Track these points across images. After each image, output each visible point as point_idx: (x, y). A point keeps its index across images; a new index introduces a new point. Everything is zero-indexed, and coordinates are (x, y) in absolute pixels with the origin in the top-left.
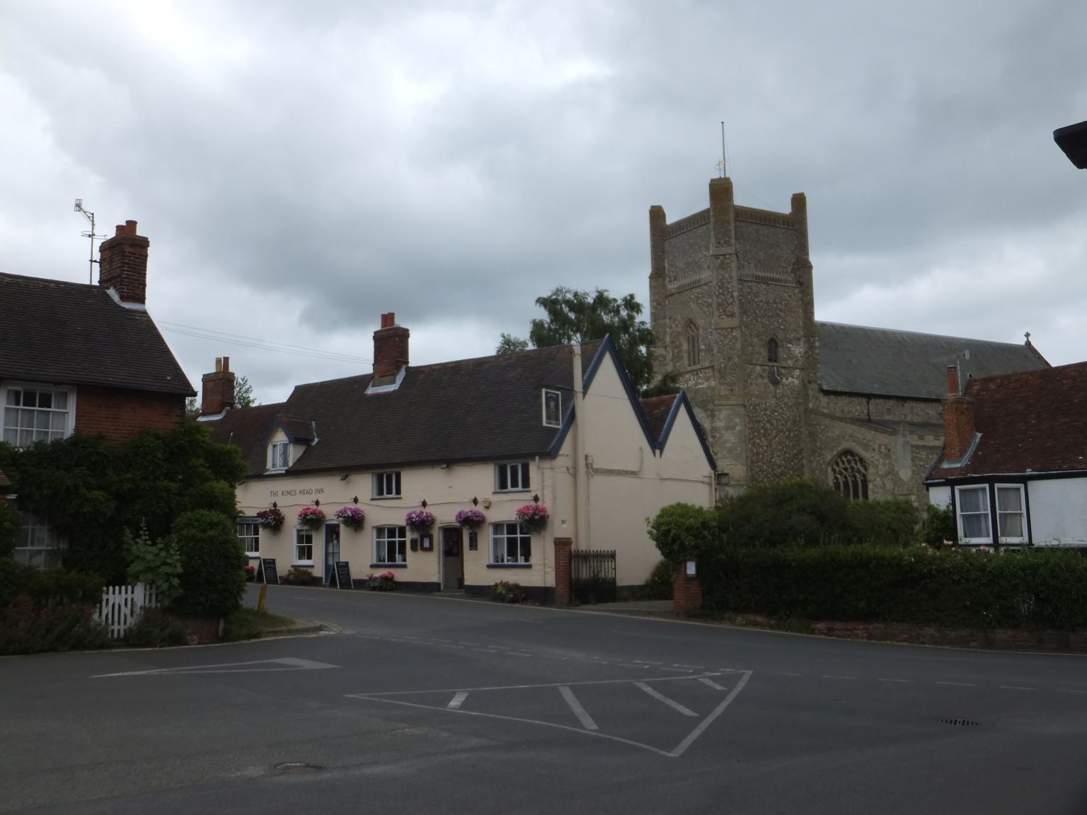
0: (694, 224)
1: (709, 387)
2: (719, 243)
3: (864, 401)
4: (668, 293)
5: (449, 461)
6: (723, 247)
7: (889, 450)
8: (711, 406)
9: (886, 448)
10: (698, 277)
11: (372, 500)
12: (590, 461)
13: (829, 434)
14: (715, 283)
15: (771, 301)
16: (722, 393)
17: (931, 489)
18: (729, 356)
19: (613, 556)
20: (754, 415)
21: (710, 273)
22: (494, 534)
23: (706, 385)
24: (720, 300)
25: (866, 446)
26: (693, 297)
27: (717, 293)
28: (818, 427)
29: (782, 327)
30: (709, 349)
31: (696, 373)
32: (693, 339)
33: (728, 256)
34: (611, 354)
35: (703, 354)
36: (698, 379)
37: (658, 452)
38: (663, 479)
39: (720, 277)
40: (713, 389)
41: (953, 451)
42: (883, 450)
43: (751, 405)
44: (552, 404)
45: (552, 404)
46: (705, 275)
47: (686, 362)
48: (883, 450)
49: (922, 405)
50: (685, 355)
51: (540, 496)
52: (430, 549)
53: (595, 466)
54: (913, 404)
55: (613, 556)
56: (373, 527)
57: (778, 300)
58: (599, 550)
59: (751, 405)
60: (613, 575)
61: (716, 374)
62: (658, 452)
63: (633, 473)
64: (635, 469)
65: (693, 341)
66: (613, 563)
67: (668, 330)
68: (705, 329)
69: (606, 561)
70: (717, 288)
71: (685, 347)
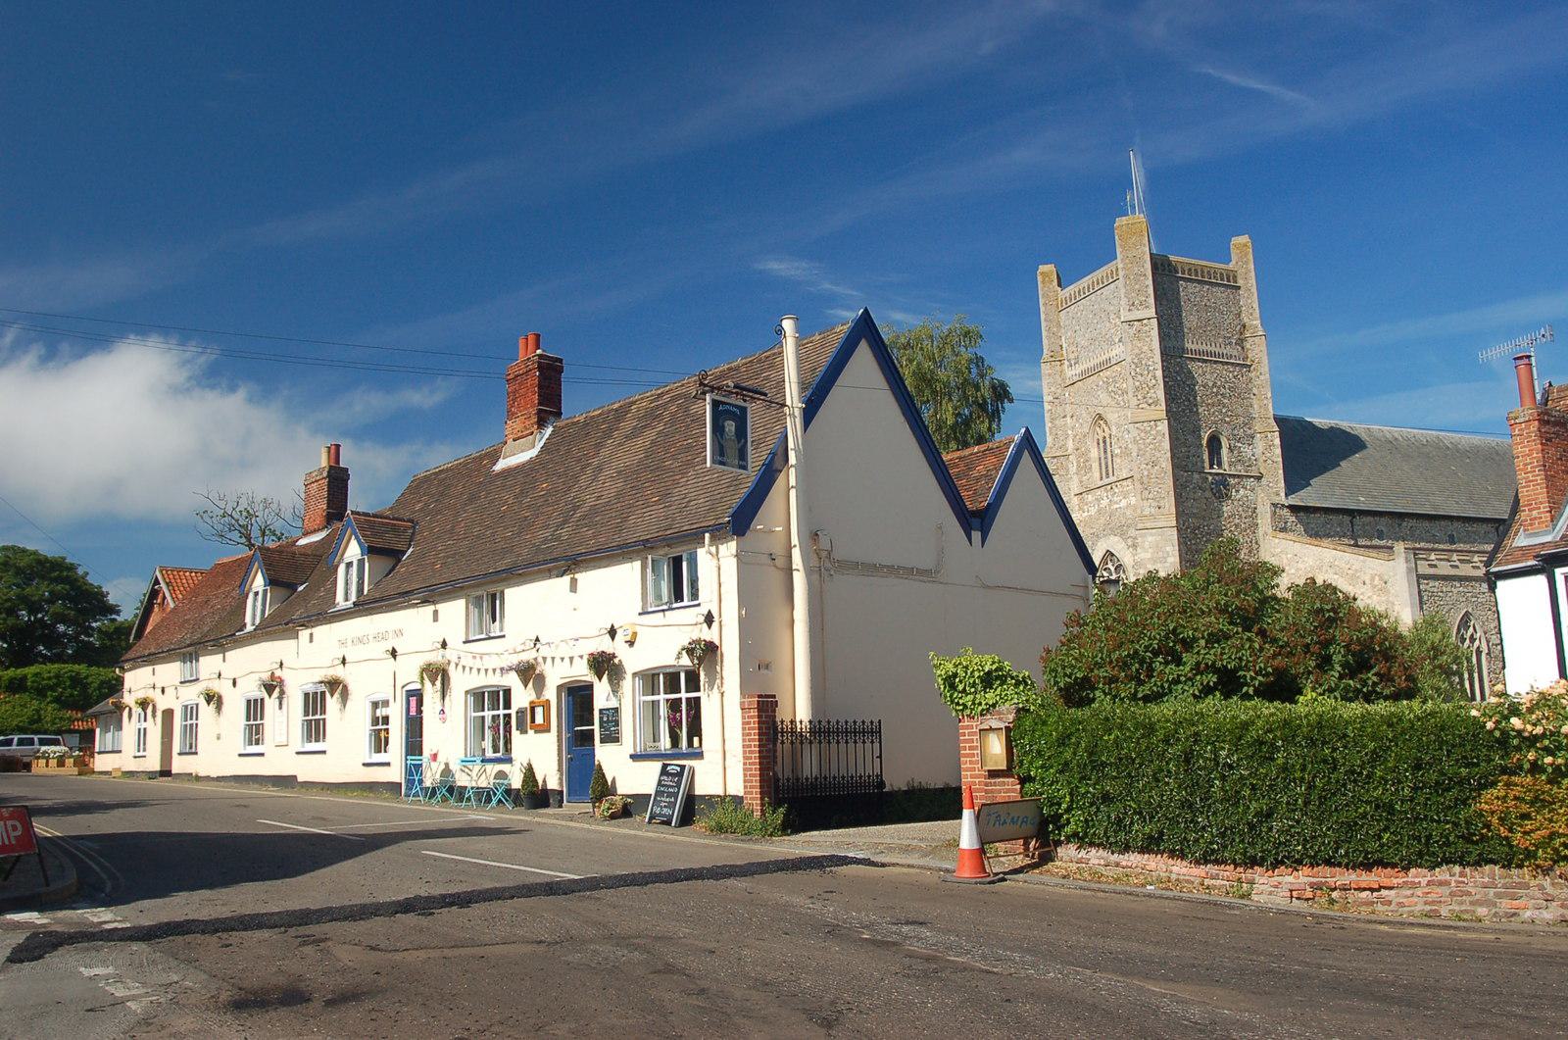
0: (1098, 284)
1: (1129, 505)
2: (1133, 304)
3: (1347, 519)
4: (1068, 382)
5: (570, 562)
6: (1138, 310)
7: (1386, 583)
8: (1132, 532)
9: (1381, 579)
10: (1107, 356)
11: (464, 642)
12: (824, 543)
13: (1300, 565)
14: (1129, 359)
15: (1211, 384)
16: (1147, 512)
17: (1500, 584)
18: (1154, 459)
19: (874, 732)
20: (1193, 542)
21: (1122, 348)
22: (699, 698)
23: (1123, 503)
24: (1137, 384)
25: (1353, 578)
26: (1101, 383)
27: (1133, 374)
28: (1284, 556)
29: (1227, 419)
30: (1126, 453)
31: (1109, 487)
32: (1104, 442)
33: (1145, 322)
34: (871, 346)
35: (1119, 461)
36: (1113, 495)
37: (976, 535)
38: (986, 587)
39: (1137, 351)
40: (1135, 508)
41: (1535, 513)
42: (1376, 582)
43: (1187, 528)
44: (730, 426)
45: (730, 426)
46: (1117, 351)
47: (1097, 475)
48: (1376, 582)
49: (1426, 524)
50: (1095, 466)
51: (715, 614)
52: (545, 729)
53: (836, 555)
54: (1412, 523)
55: (874, 732)
56: (467, 692)
57: (1219, 383)
58: (833, 721)
59: (1187, 528)
60: (877, 771)
61: (1138, 486)
62: (976, 535)
63: (922, 572)
64: (927, 563)
65: (1104, 444)
66: (877, 745)
67: (1070, 432)
68: (1119, 426)
69: (843, 741)
70: (1133, 366)
71: (1094, 453)
